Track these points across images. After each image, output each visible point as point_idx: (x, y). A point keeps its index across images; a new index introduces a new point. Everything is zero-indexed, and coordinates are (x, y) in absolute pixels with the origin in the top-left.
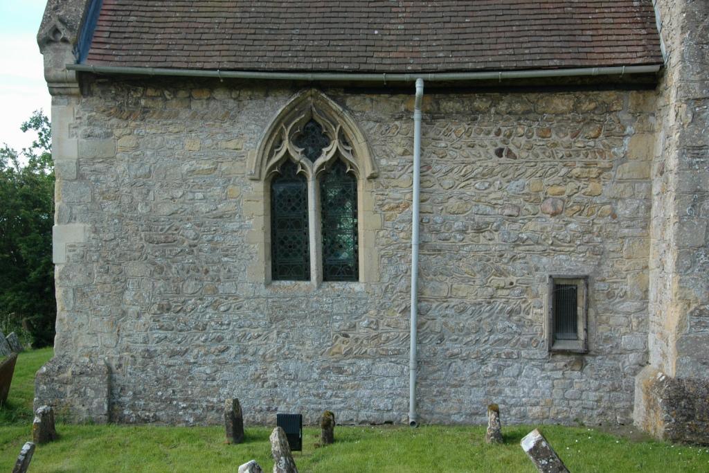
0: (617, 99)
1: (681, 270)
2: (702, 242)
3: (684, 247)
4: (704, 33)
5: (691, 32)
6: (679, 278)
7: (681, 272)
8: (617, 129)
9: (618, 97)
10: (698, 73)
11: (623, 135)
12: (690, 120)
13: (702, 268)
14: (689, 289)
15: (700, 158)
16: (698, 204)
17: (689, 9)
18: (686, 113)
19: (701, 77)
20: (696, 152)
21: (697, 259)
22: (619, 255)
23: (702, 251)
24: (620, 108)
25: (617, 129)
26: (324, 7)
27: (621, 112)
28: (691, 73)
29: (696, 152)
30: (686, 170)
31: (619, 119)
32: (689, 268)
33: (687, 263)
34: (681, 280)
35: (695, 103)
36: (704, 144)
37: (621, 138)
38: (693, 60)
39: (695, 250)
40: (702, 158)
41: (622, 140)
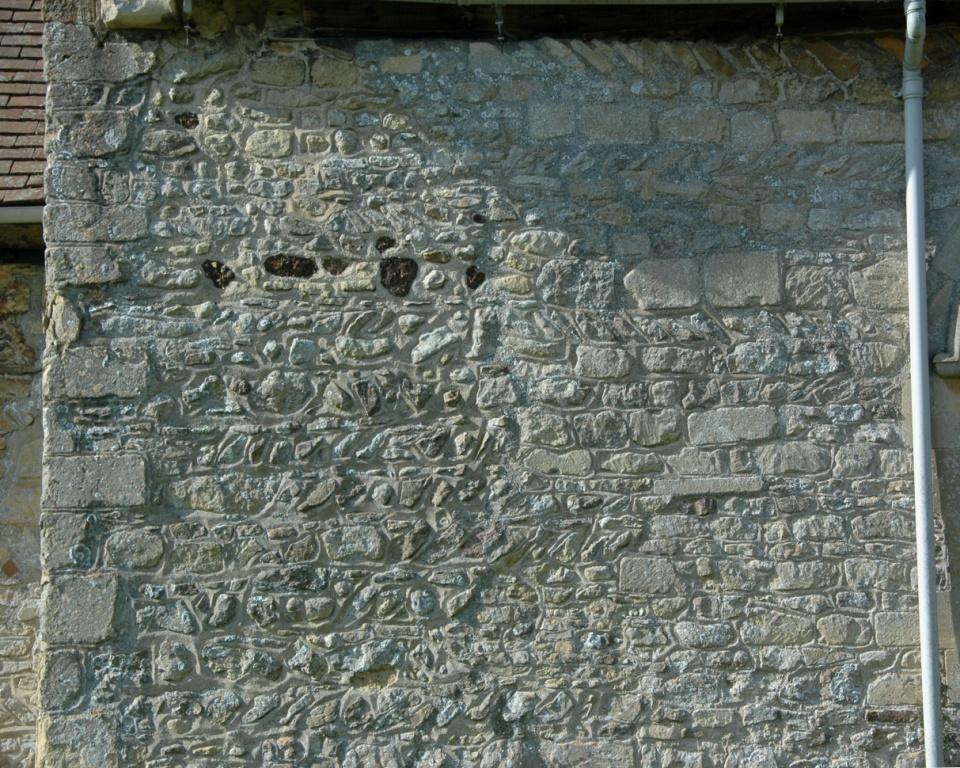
0: (16, 285)
1: (53, 703)
2: (103, 632)
3: (63, 644)
4: (96, 132)
5: (67, 129)
6: (50, 722)
7: (54, 708)
8: (18, 357)
9: (16, 282)
10: (88, 225)
11: (30, 369)
12: (73, 336)
13: (108, 695)
14: (73, 750)
15: (100, 424)
16: (99, 538)
17: (57, 76)
18: (64, 319)
19: (94, 233)
20: (91, 411)
21: (97, 672)
22: (23, 665)
23: (108, 653)
24: (22, 307)
25: (18, 357)
26: (23, 108)
27: (26, 316)
28: (72, 223)
29: (91, 411)
30: (70, 454)
31: (20, 334)
32: (74, 697)
33: (70, 679)
34: (53, 726)
35: (87, 294)
36: (107, 391)
37: (27, 377)
38: (73, 194)
39: (89, 649)
40: (106, 425)
41: (29, 383)
